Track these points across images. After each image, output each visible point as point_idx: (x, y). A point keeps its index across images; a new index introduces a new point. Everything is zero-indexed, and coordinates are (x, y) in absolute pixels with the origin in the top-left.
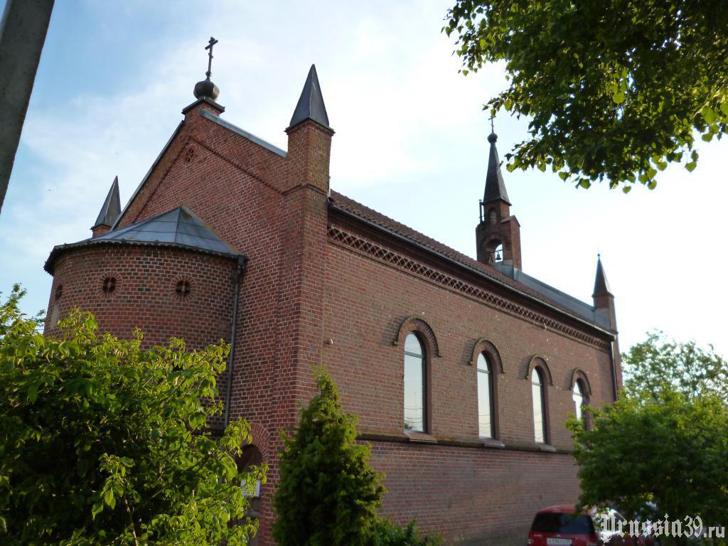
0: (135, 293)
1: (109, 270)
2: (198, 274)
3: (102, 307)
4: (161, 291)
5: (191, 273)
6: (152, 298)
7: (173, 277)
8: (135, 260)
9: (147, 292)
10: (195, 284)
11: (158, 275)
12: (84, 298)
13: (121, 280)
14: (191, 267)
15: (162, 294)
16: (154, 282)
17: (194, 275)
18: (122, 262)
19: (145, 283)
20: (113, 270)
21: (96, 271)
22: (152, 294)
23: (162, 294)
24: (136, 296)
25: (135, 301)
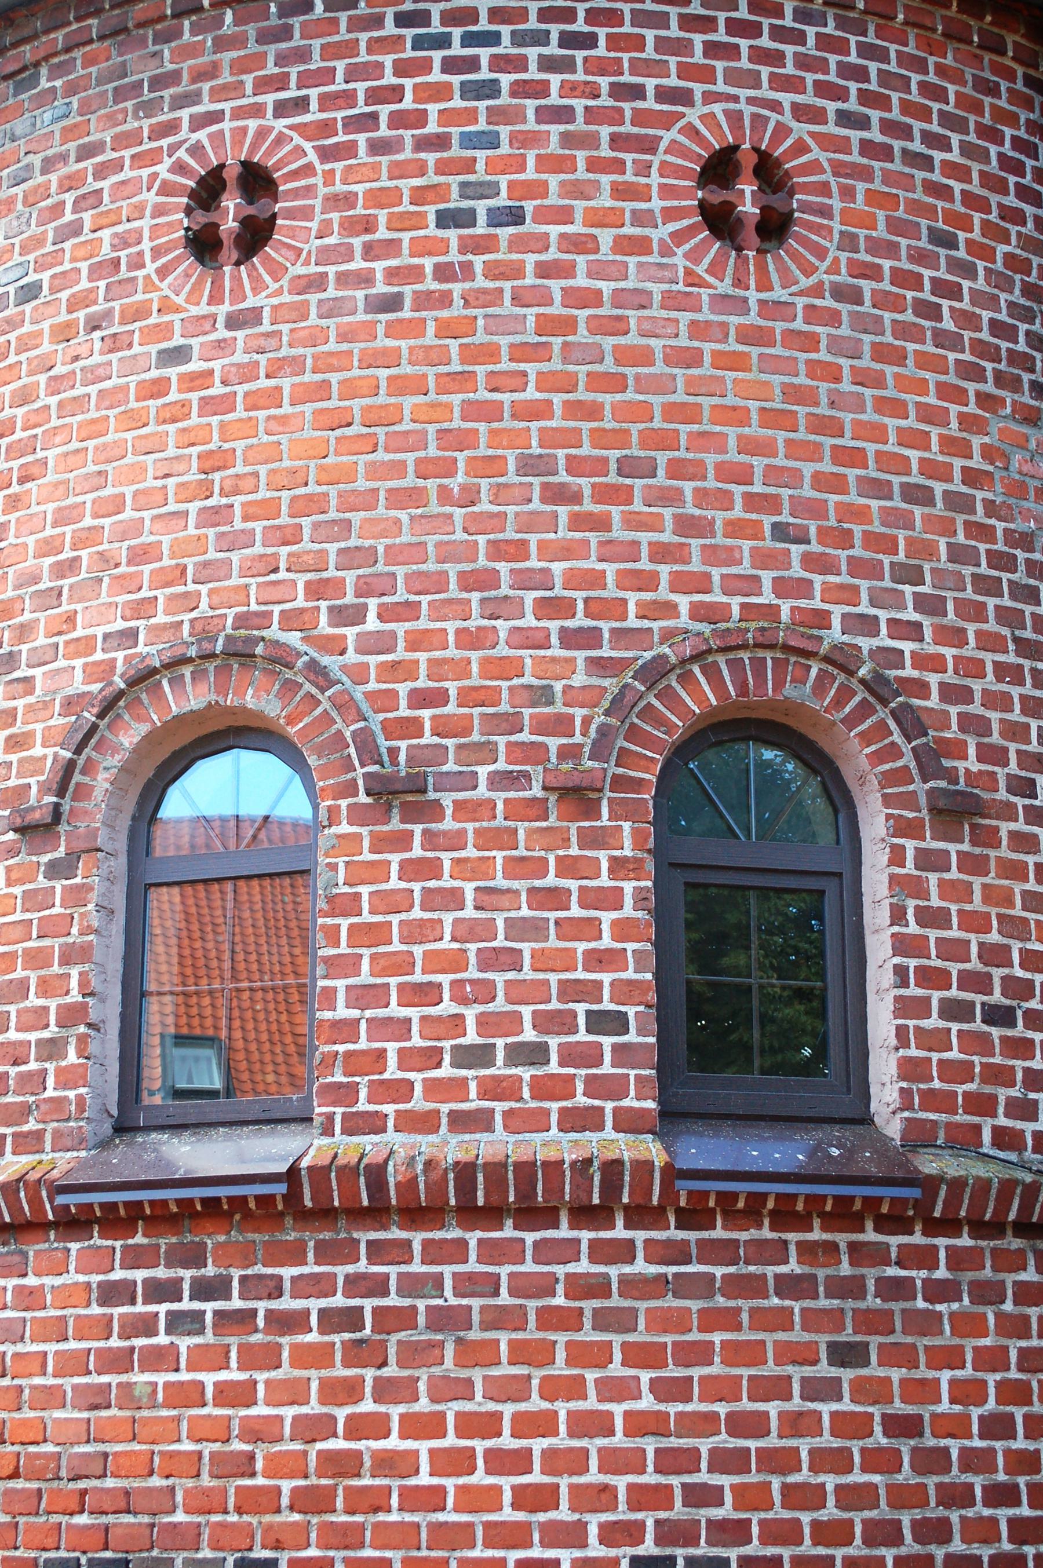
0: (421, 248)
1: (216, 117)
2: (831, 107)
3: (195, 366)
4: (599, 219)
5: (786, 98)
6: (545, 270)
7: (667, 121)
8: (390, 28)
9: (505, 233)
10: (815, 167)
11: (564, 114)
12: (64, 333)
13: (308, 170)
14: (775, 58)
15: (606, 237)
16: (546, 164)
17: (800, 112)
18: (302, 55)
19: (480, 173)
20: (238, 113)
21: (122, 141)
22: (542, 243)
23: (606, 237)
24: (428, 263)
25: (424, 300)
